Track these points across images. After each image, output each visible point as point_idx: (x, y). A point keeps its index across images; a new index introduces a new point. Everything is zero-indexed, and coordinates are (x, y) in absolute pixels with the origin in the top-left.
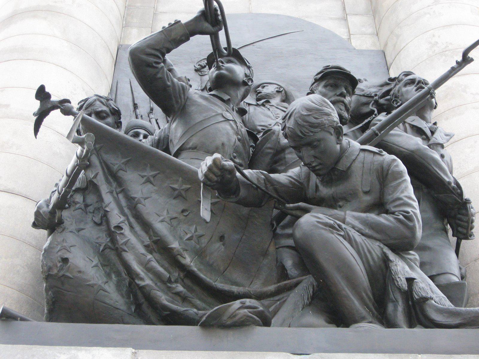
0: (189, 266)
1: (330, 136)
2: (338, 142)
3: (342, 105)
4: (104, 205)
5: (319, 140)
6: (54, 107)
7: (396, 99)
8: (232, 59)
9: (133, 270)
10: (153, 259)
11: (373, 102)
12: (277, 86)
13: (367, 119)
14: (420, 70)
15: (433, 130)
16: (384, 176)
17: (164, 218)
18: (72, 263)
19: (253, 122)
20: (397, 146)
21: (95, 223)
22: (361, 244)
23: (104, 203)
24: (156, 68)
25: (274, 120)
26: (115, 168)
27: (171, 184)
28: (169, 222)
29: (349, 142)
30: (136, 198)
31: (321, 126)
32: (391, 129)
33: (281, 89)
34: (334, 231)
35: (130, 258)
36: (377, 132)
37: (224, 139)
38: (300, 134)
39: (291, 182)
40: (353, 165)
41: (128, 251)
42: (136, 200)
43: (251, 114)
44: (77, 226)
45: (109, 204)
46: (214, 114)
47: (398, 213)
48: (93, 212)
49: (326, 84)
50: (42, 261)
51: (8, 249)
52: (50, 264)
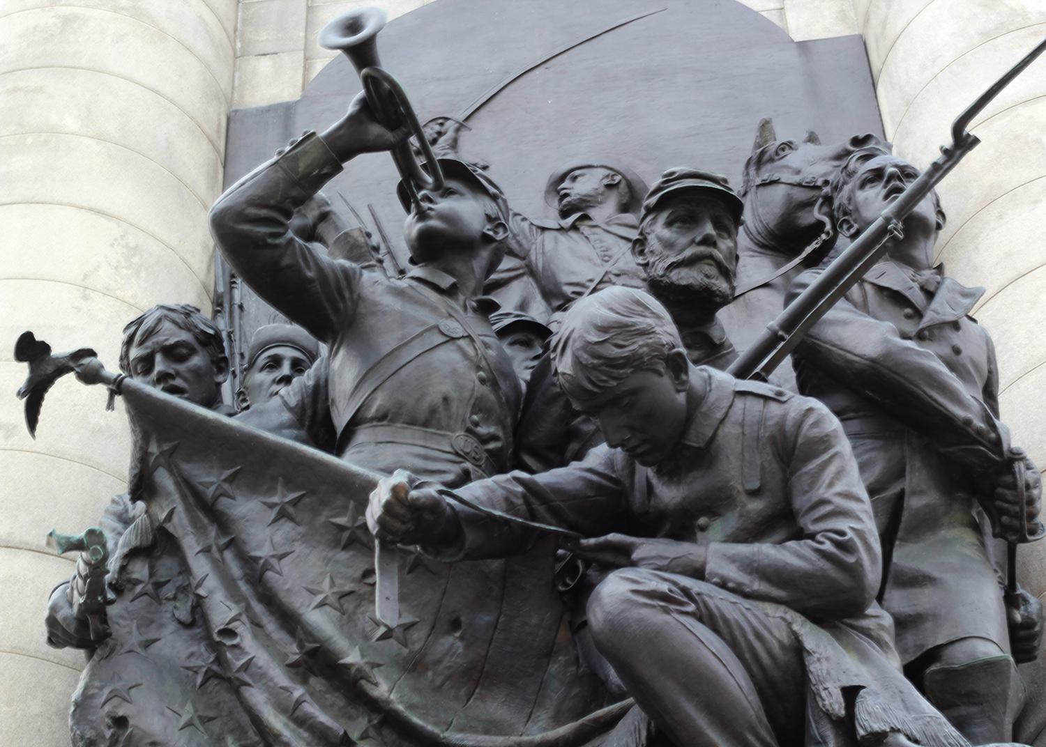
0: (388, 702)
1: (656, 379)
2: (679, 388)
3: (710, 265)
4: (194, 583)
5: (634, 392)
6: (61, 369)
7: (846, 218)
8: (452, 184)
9: (266, 727)
10: (307, 697)
11: (820, 201)
12: (607, 172)
13: (809, 243)
14: (939, 92)
15: (931, 288)
16: (791, 452)
17: (326, 598)
18: (136, 727)
19: (553, 275)
20: (841, 349)
21: (180, 622)
22: (737, 621)
23: (193, 578)
24: (276, 246)
25: (598, 266)
26: (210, 491)
27: (332, 517)
28: (337, 605)
29: (710, 377)
30: (260, 558)
31: (635, 362)
32: (830, 304)
33: (618, 178)
34: (672, 607)
35: (257, 697)
36: (781, 333)
37: (446, 387)
38: (590, 387)
39: (590, 483)
40: (720, 433)
41: (253, 684)
42: (262, 562)
43: (549, 254)
44: (140, 634)
45: (203, 579)
46: (420, 330)
47: (823, 536)
48: (175, 598)
49: (670, 219)
50: (72, 730)
51: (12, 682)
52: (90, 734)
